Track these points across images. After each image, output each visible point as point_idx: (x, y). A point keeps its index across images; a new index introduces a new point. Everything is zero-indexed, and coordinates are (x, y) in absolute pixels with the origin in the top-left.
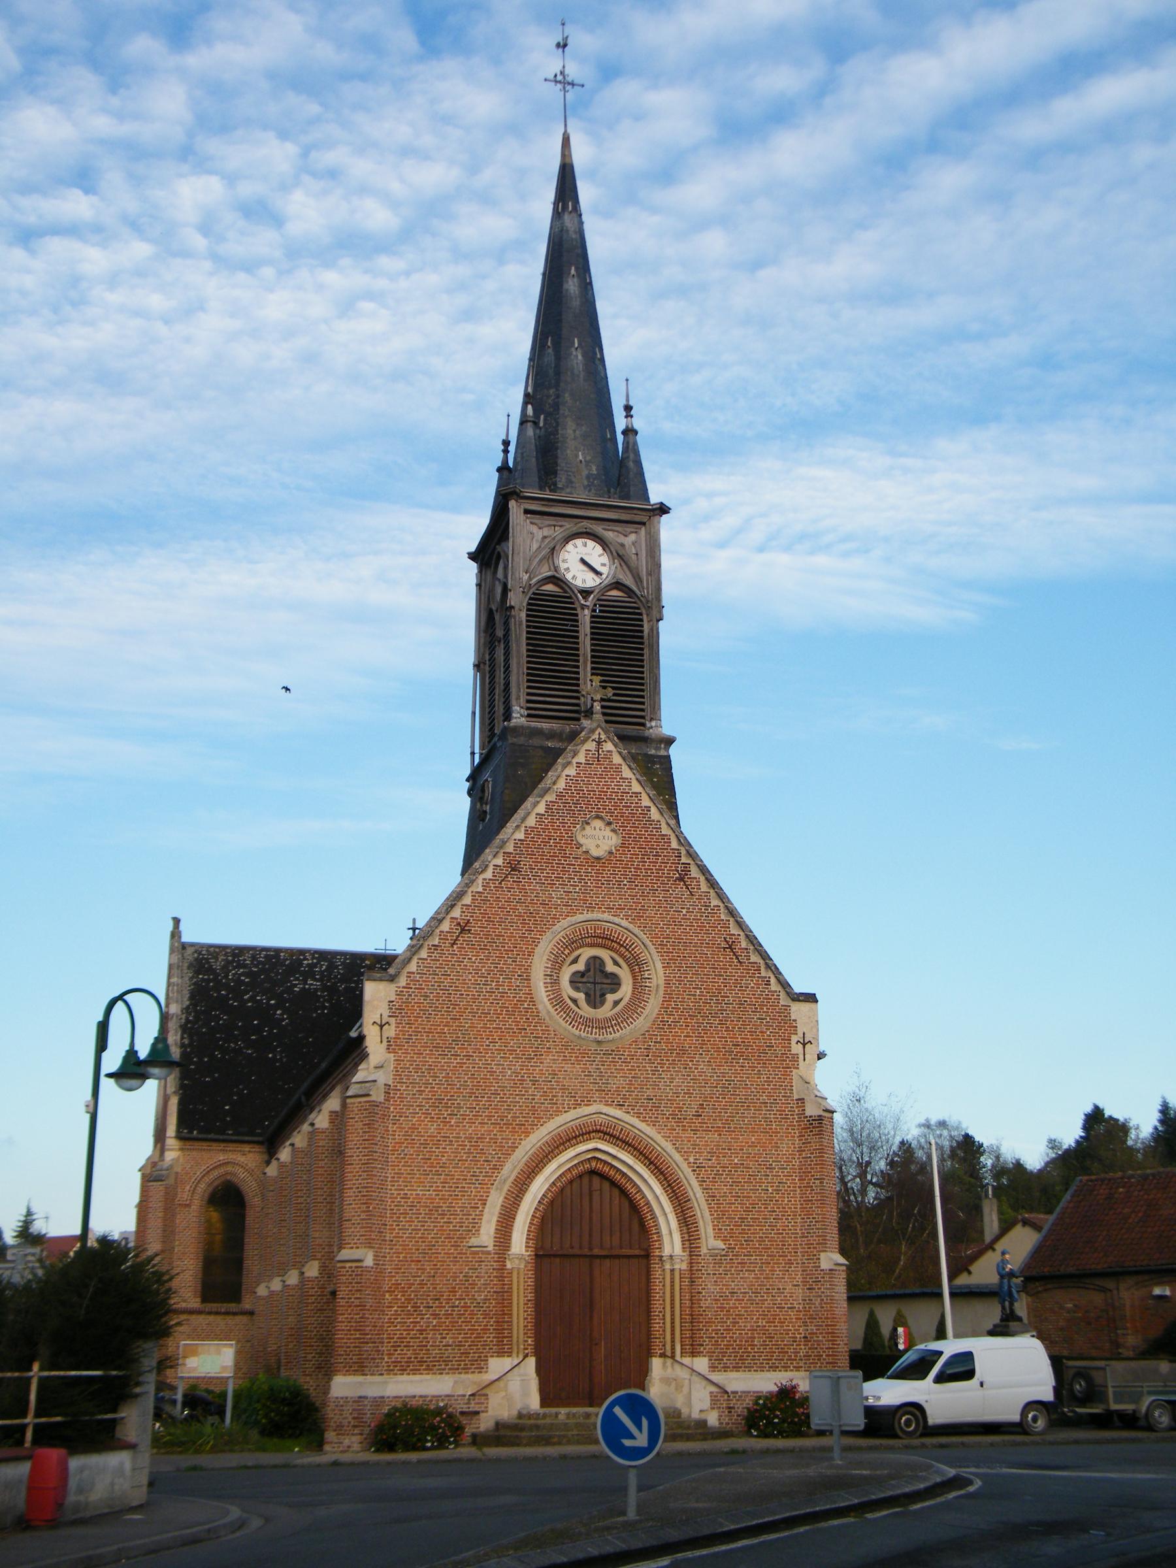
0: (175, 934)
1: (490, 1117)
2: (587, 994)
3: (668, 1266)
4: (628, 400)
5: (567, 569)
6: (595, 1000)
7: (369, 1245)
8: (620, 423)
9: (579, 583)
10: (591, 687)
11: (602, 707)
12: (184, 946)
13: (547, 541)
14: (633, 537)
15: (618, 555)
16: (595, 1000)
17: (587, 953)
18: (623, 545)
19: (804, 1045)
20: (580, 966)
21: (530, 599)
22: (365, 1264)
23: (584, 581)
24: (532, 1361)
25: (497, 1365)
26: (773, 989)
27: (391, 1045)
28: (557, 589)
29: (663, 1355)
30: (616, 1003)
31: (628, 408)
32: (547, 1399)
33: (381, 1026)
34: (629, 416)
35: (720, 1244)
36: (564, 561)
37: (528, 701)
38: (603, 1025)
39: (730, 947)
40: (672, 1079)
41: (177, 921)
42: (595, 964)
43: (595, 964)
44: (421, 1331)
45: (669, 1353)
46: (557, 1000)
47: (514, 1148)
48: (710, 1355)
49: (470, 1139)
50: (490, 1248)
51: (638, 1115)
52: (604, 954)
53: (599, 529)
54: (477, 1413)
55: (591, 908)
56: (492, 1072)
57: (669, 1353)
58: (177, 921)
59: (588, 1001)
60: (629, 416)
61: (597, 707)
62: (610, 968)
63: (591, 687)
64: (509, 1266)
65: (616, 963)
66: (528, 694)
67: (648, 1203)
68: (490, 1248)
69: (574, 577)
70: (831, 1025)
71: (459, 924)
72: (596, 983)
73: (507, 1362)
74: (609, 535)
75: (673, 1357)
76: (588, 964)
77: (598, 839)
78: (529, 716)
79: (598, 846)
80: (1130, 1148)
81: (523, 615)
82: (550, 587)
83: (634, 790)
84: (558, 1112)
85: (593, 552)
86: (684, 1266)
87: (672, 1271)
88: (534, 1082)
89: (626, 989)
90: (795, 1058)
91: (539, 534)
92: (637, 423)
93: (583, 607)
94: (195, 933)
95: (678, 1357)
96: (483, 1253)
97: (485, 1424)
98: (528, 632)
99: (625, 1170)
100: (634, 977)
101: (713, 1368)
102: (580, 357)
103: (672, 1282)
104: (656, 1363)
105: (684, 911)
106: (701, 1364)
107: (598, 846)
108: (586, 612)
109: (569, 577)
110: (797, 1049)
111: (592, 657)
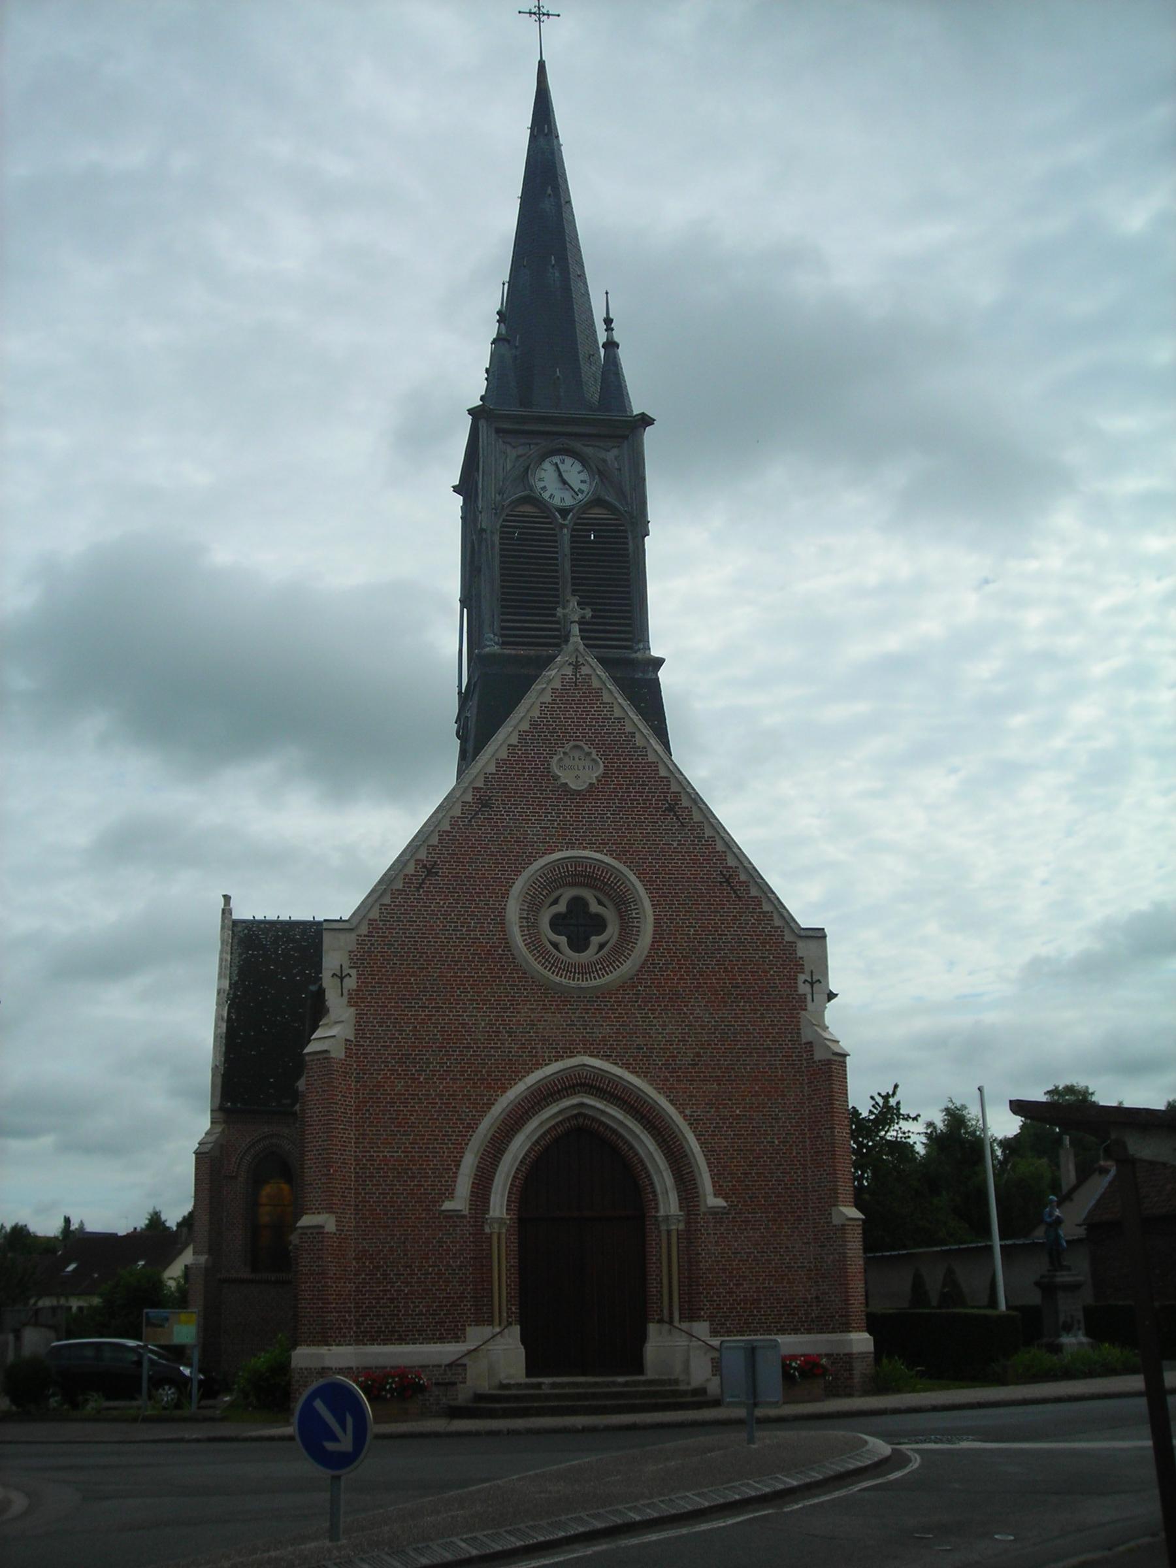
0: (226, 912)
1: (462, 1073)
2: (569, 938)
3: (663, 1227)
4: (608, 313)
5: (544, 488)
6: (579, 945)
7: (330, 1209)
8: (602, 337)
9: (557, 502)
10: (572, 611)
11: (581, 630)
12: (235, 923)
13: (521, 459)
14: (615, 452)
15: (600, 473)
16: (579, 945)
17: (569, 893)
18: (604, 461)
19: (812, 984)
20: (561, 907)
21: (504, 521)
22: (326, 1230)
23: (562, 500)
24: (516, 1329)
25: (476, 1335)
26: (777, 924)
27: (354, 1000)
28: (534, 510)
29: (661, 1321)
30: (602, 946)
31: (608, 321)
32: (533, 1366)
33: (342, 979)
34: (609, 329)
35: (720, 1202)
36: (540, 480)
37: (503, 628)
38: (585, 971)
39: (727, 881)
40: (664, 1026)
41: (227, 898)
42: (577, 904)
43: (577, 904)
44: (392, 1300)
45: (666, 1318)
46: (534, 943)
47: (489, 1105)
48: (711, 1318)
49: (441, 1096)
50: (466, 1212)
51: (627, 1066)
52: (587, 894)
53: (577, 445)
54: (453, 1384)
55: (571, 845)
56: (463, 1025)
57: (666, 1318)
58: (227, 898)
59: (570, 945)
60: (609, 329)
61: (575, 629)
62: (595, 908)
63: (572, 611)
64: (487, 1230)
65: (600, 903)
66: (503, 621)
67: (641, 1161)
68: (466, 1212)
69: (551, 496)
70: (843, 970)
71: (424, 866)
72: (578, 925)
73: (487, 1331)
74: (589, 451)
75: (671, 1322)
76: (569, 905)
77: (578, 772)
78: (504, 643)
79: (577, 777)
80: (73, 1232)
81: (496, 538)
82: (528, 509)
83: (616, 715)
84: (538, 1066)
85: (574, 472)
86: (682, 1226)
87: (669, 1232)
88: (510, 1034)
89: (612, 930)
90: (802, 999)
91: (512, 453)
92: (617, 336)
93: (562, 526)
94: (242, 912)
95: (677, 1324)
96: (458, 1217)
97: (463, 1395)
98: (502, 556)
99: (615, 1126)
100: (621, 918)
101: (714, 1333)
102: (557, 274)
103: (669, 1244)
104: (652, 1328)
105: (675, 844)
106: (701, 1328)
107: (577, 777)
108: (565, 531)
109: (546, 495)
110: (803, 988)
111: (573, 578)
